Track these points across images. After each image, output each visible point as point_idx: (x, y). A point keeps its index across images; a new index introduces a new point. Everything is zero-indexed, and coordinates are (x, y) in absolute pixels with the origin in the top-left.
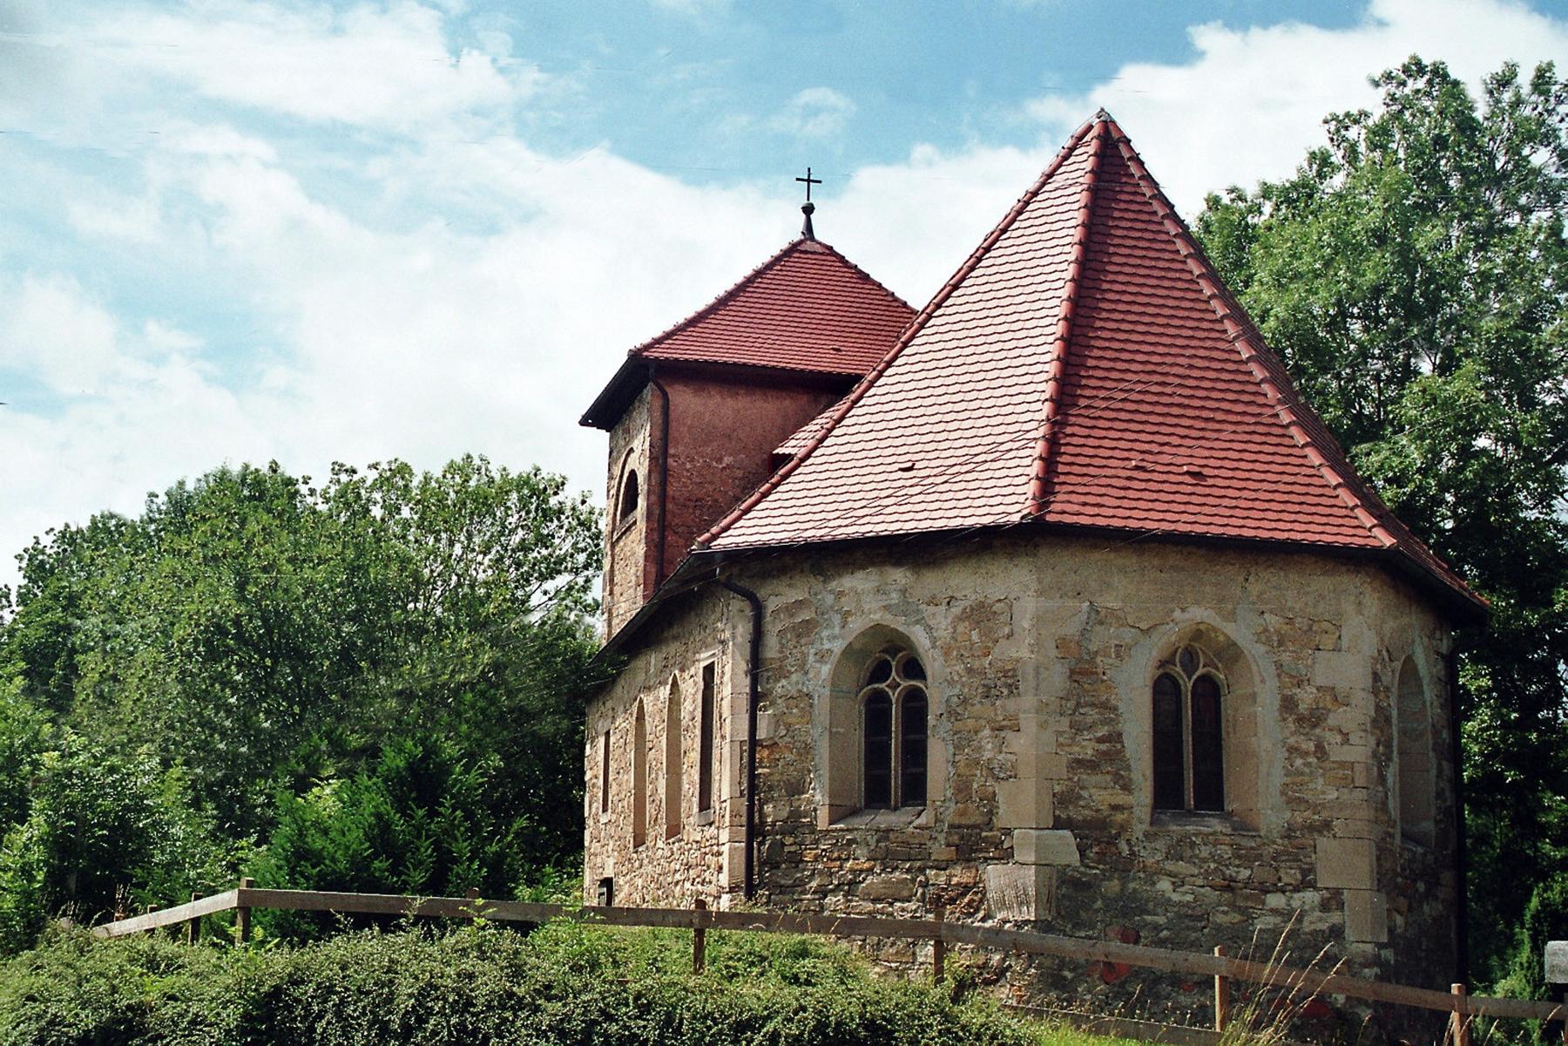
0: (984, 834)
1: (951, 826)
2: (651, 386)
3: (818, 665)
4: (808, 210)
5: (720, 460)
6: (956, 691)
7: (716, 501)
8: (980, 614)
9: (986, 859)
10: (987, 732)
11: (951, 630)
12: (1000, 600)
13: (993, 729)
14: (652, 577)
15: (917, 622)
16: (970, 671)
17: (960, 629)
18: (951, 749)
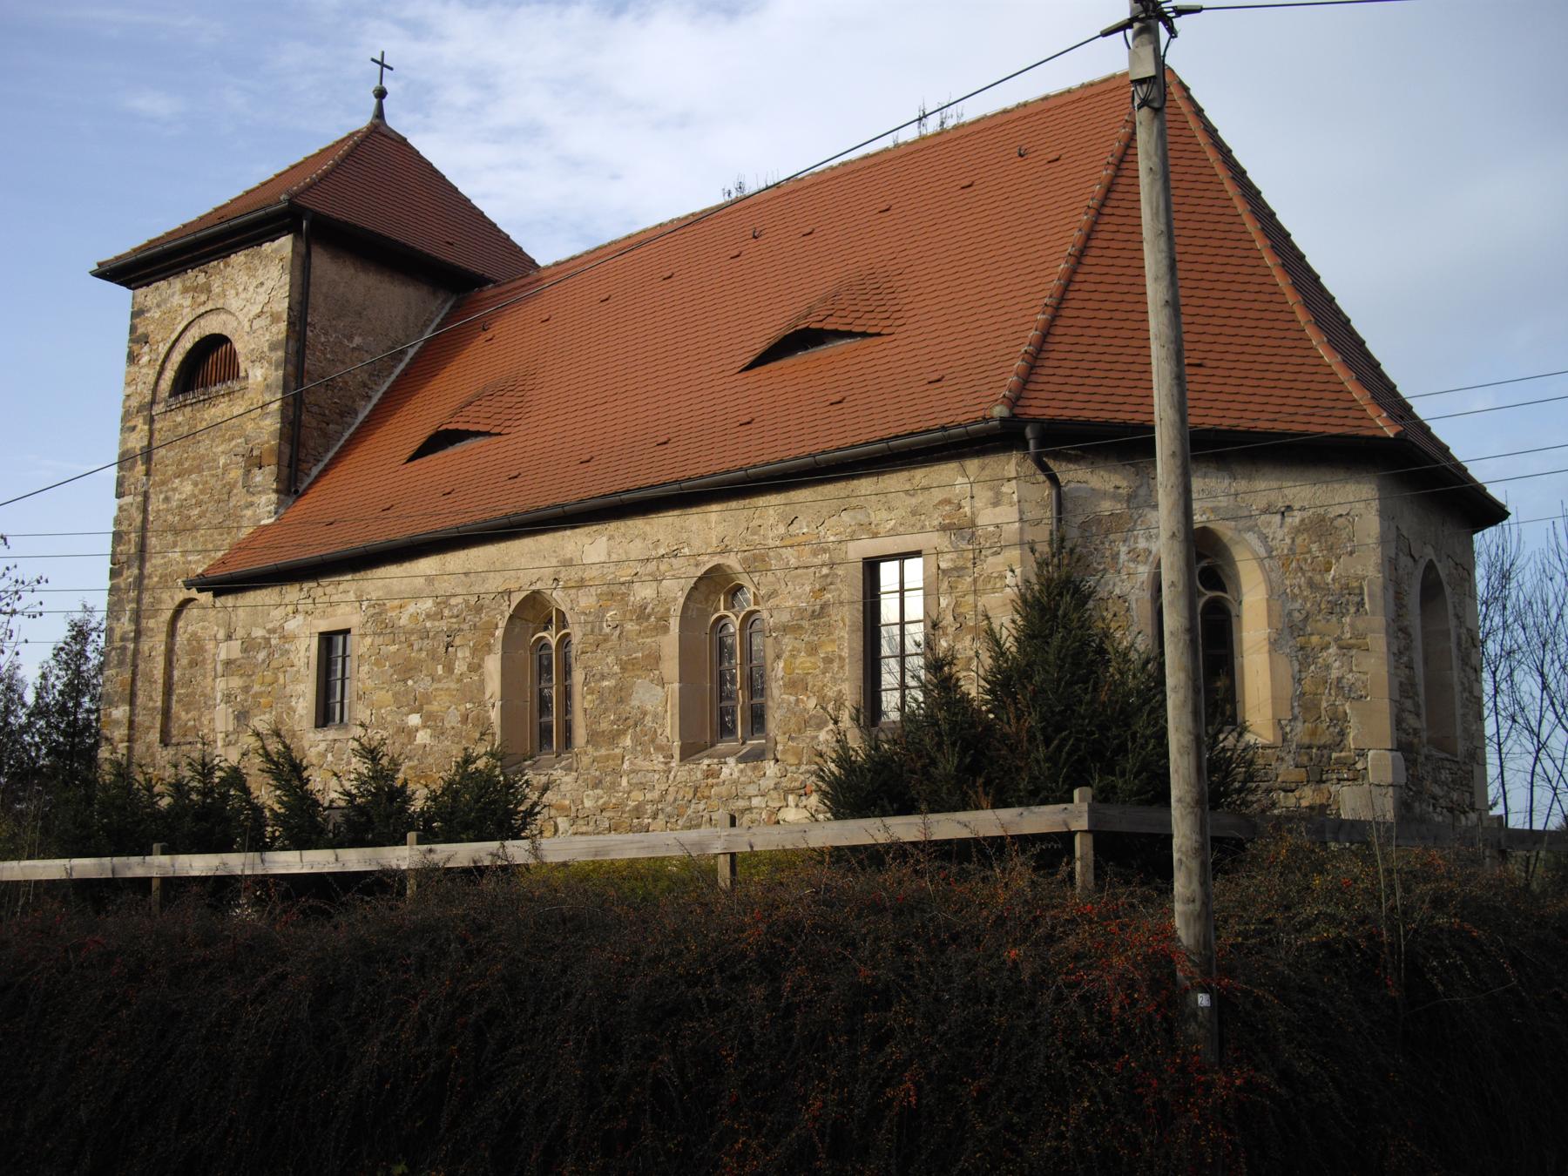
0: (1334, 755)
1: (1300, 747)
2: (285, 243)
3: (1132, 565)
4: (381, 94)
5: (350, 338)
6: (1297, 605)
7: (346, 383)
8: (1321, 527)
9: (1339, 780)
10: (1333, 650)
11: (1288, 541)
12: (1341, 516)
13: (1341, 648)
14: (286, 458)
15: (1250, 529)
16: (1311, 584)
17: (1299, 541)
18: (1297, 667)
